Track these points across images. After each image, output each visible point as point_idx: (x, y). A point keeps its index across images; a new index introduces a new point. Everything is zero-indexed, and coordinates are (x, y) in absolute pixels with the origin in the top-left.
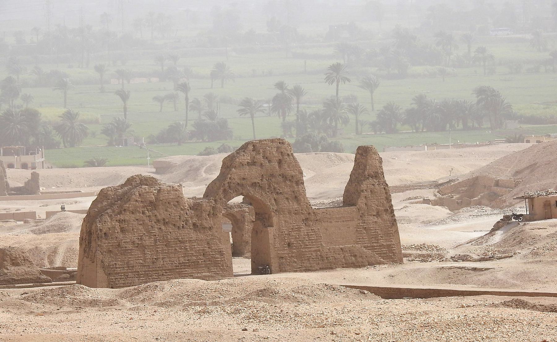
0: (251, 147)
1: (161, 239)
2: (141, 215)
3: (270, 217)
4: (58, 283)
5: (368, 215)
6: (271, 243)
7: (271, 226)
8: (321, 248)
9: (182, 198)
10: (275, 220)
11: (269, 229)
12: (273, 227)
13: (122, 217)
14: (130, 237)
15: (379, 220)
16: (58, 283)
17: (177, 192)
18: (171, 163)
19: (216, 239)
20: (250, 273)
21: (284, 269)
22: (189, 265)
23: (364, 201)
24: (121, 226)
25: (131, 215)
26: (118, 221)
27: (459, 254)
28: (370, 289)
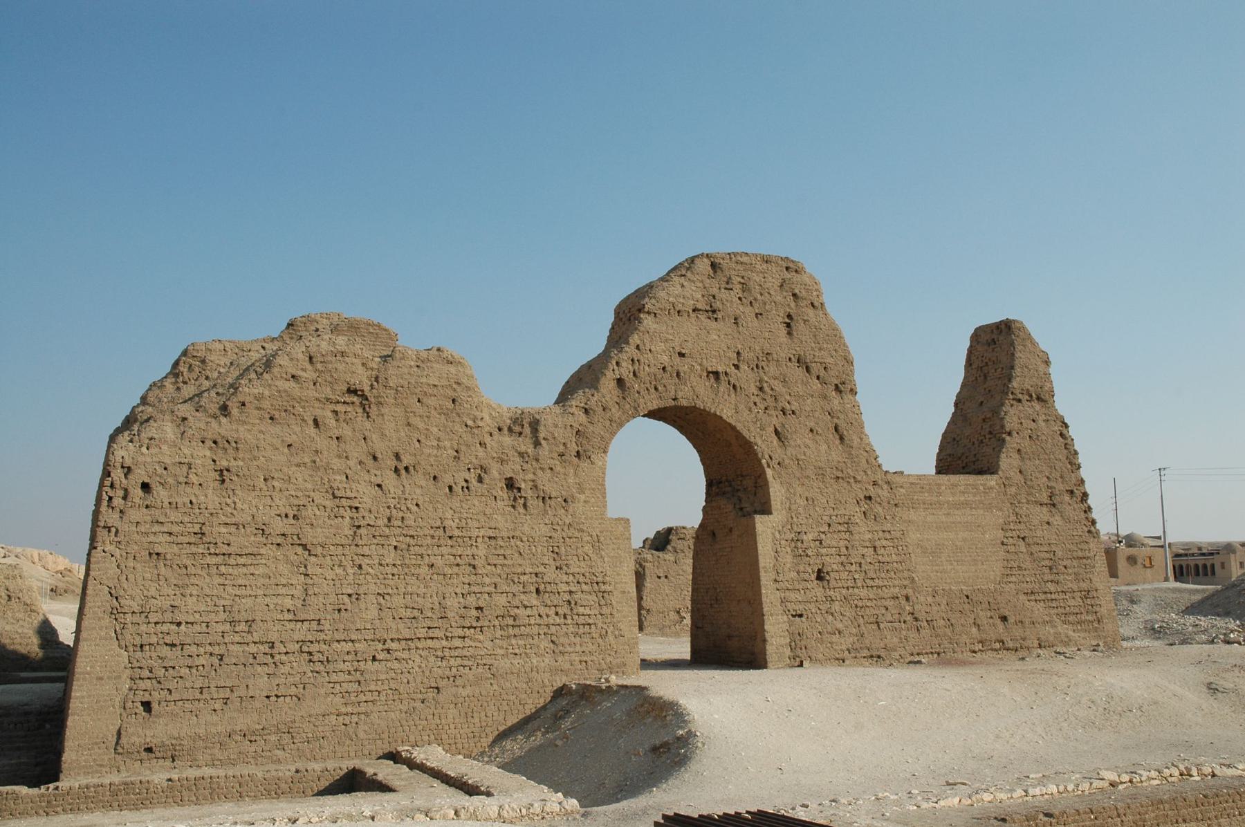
0: (703, 266)
1: (380, 522)
2: (312, 431)
3: (760, 484)
4: (53, 674)
5: (1028, 502)
6: (765, 567)
7: (766, 510)
8: (911, 591)
9: (468, 388)
10: (776, 491)
11: (758, 519)
12: (771, 513)
13: (224, 427)
14: (247, 504)
15: (1057, 520)
16: (53, 674)
17: (452, 369)
18: (689, 714)
19: (585, 539)
20: (688, 656)
21: (807, 653)
22: (481, 627)
23: (1015, 461)
24: (218, 463)
25: (266, 425)
26: (209, 443)
27: (1007, 613)
28: (109, 447)
